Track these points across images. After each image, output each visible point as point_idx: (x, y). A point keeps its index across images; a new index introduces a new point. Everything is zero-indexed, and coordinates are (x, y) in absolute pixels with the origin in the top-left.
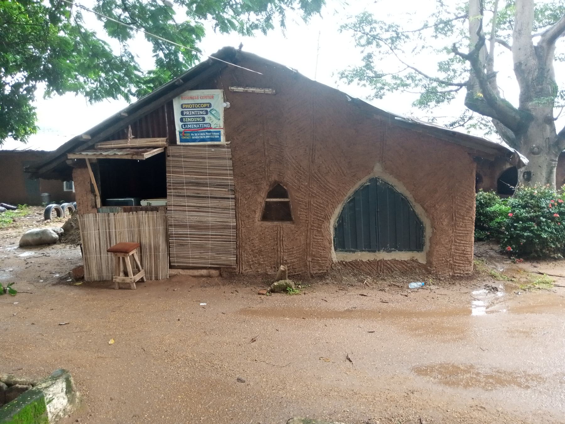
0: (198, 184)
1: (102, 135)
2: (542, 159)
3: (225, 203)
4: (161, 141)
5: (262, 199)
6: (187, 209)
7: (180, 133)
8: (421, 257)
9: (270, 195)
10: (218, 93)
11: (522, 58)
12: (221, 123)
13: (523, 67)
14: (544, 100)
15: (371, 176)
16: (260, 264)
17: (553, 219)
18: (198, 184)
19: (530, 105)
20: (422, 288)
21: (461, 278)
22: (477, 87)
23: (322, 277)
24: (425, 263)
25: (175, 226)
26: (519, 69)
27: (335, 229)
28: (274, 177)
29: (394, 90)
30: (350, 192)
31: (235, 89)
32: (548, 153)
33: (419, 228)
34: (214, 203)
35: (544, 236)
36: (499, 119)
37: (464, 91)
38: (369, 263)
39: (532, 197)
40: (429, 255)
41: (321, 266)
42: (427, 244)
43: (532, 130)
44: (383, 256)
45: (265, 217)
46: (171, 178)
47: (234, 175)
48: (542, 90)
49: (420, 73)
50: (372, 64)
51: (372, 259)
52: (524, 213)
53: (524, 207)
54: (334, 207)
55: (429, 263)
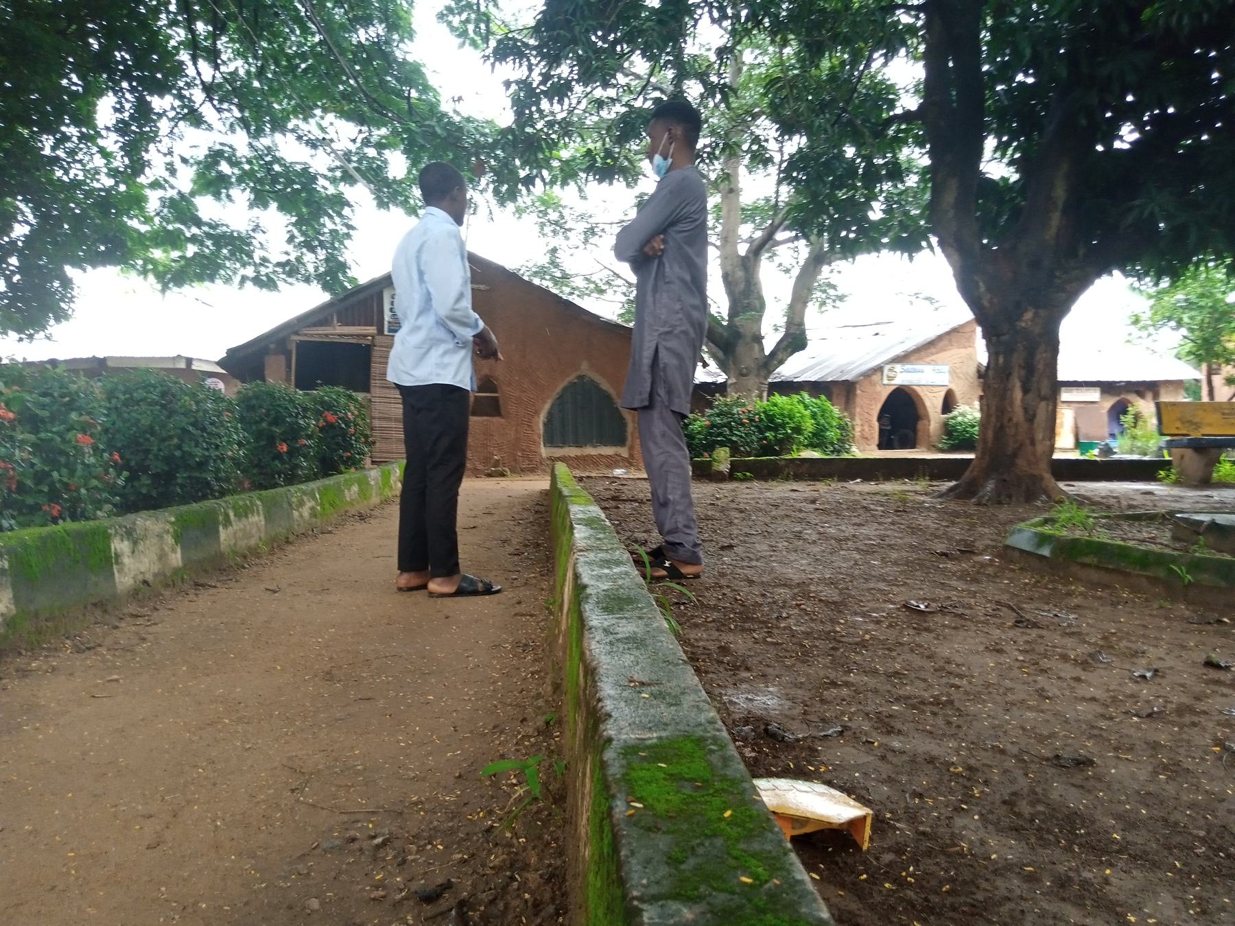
4: (372, 330)
6: (392, 401)
7: (389, 322)
8: (624, 452)
11: (729, 268)
13: (730, 278)
15: (578, 373)
17: (743, 424)
23: (532, 470)
24: (627, 456)
25: (380, 418)
27: (545, 424)
29: (586, 297)
32: (758, 375)
35: (734, 439)
38: (577, 458)
41: (531, 461)
43: (740, 349)
44: (590, 451)
49: (619, 276)
50: (558, 260)
51: (579, 454)
52: (718, 420)
53: (718, 415)
54: (545, 402)
55: (631, 456)
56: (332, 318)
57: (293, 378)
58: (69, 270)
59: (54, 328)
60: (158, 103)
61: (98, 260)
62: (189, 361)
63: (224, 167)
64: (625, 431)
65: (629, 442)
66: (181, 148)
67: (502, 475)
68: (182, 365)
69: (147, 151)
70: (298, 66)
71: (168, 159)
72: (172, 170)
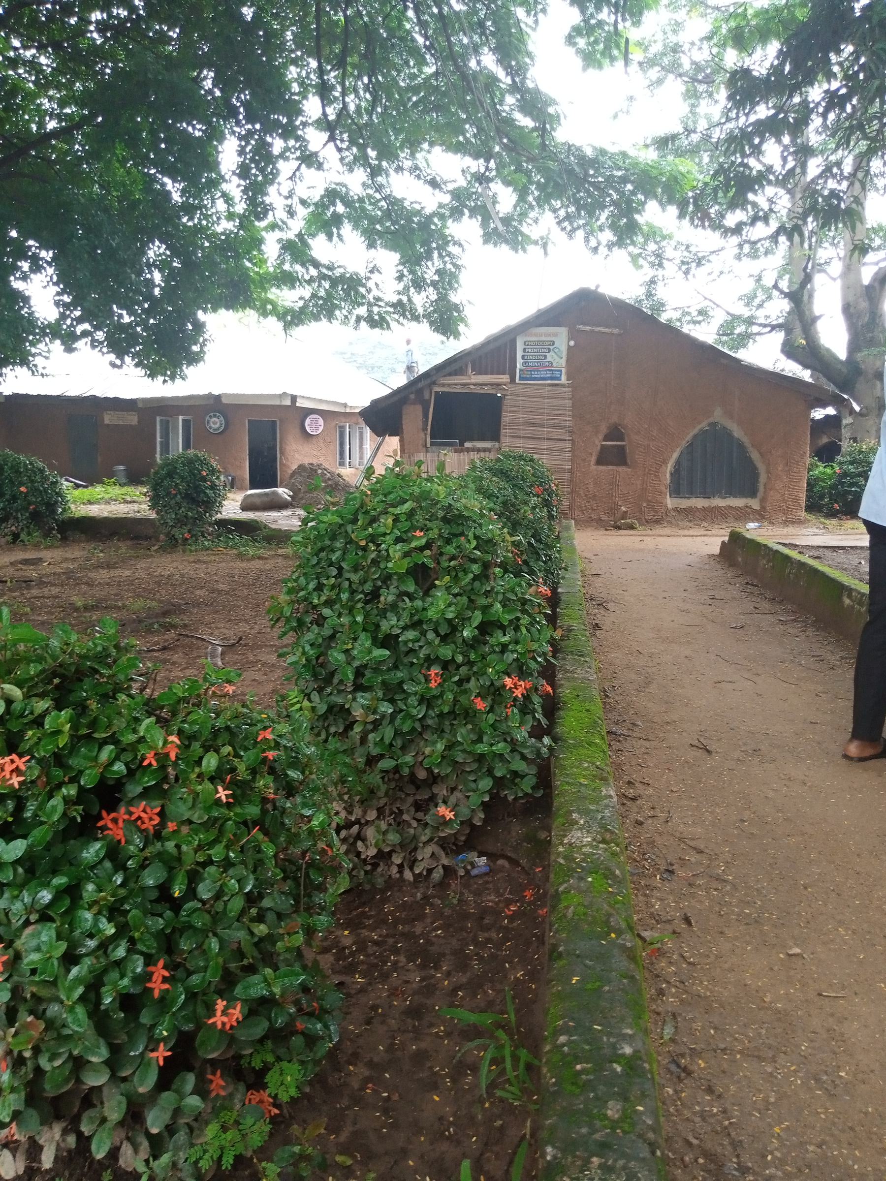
0: (534, 425)
1: (448, 370)
2: (871, 422)
3: (561, 445)
4: (505, 378)
5: (598, 442)
8: (755, 504)
9: (606, 439)
10: (563, 331)
12: (563, 362)
13: (852, 310)
14: (875, 351)
15: (711, 420)
16: (593, 510)
18: (534, 425)
19: (859, 356)
20: (759, 527)
21: (793, 523)
22: (798, 330)
23: (658, 522)
26: (847, 309)
27: (671, 474)
28: (615, 419)
30: (689, 437)
31: (581, 327)
33: (754, 474)
34: (551, 444)
36: (820, 372)
37: (779, 337)
38: (704, 509)
39: (860, 452)
40: (763, 501)
42: (761, 488)
44: (718, 502)
45: (599, 462)
46: (507, 417)
47: (574, 416)
48: (872, 338)
51: (706, 505)
53: (852, 463)
54: (673, 451)
55: (763, 508)
56: (467, 366)
57: (429, 427)
58: (200, 315)
59: (190, 371)
60: (277, 145)
61: (231, 305)
62: (294, 398)
63: (340, 208)
64: (757, 481)
65: (760, 494)
66: (302, 191)
67: (631, 527)
68: (288, 402)
69: (267, 194)
70: (409, 99)
71: (289, 202)
72: (291, 213)
